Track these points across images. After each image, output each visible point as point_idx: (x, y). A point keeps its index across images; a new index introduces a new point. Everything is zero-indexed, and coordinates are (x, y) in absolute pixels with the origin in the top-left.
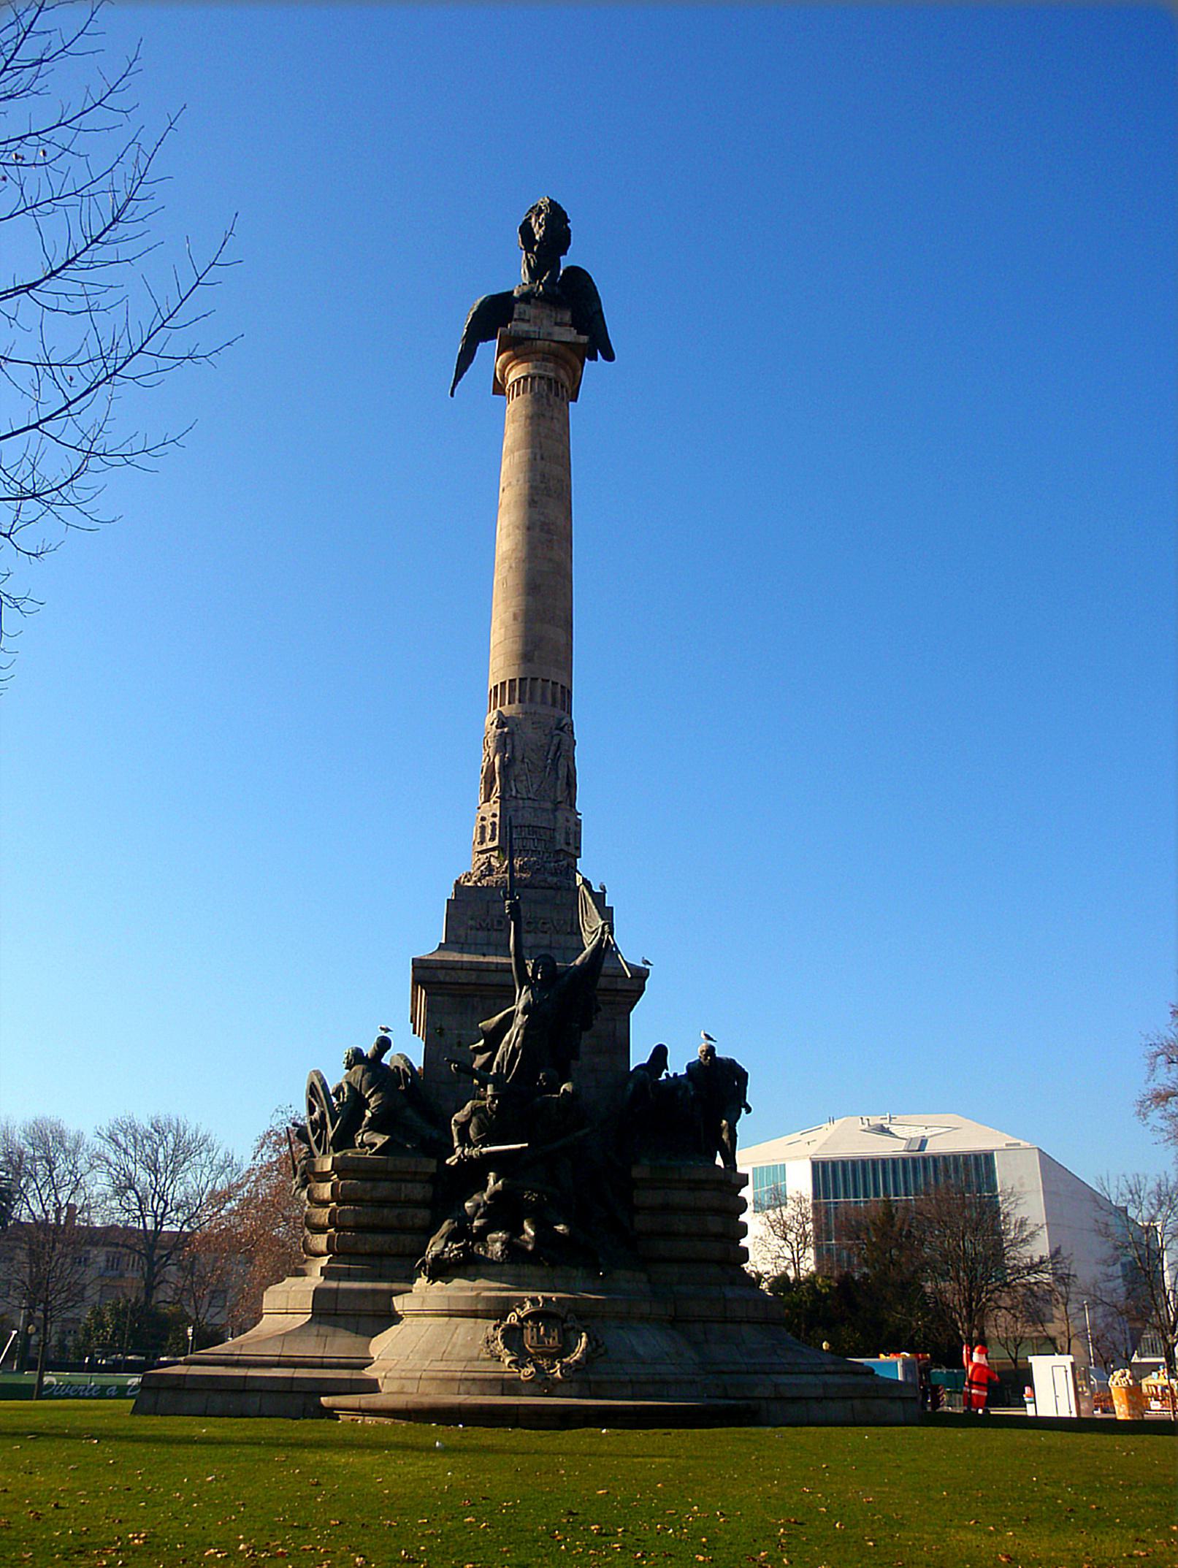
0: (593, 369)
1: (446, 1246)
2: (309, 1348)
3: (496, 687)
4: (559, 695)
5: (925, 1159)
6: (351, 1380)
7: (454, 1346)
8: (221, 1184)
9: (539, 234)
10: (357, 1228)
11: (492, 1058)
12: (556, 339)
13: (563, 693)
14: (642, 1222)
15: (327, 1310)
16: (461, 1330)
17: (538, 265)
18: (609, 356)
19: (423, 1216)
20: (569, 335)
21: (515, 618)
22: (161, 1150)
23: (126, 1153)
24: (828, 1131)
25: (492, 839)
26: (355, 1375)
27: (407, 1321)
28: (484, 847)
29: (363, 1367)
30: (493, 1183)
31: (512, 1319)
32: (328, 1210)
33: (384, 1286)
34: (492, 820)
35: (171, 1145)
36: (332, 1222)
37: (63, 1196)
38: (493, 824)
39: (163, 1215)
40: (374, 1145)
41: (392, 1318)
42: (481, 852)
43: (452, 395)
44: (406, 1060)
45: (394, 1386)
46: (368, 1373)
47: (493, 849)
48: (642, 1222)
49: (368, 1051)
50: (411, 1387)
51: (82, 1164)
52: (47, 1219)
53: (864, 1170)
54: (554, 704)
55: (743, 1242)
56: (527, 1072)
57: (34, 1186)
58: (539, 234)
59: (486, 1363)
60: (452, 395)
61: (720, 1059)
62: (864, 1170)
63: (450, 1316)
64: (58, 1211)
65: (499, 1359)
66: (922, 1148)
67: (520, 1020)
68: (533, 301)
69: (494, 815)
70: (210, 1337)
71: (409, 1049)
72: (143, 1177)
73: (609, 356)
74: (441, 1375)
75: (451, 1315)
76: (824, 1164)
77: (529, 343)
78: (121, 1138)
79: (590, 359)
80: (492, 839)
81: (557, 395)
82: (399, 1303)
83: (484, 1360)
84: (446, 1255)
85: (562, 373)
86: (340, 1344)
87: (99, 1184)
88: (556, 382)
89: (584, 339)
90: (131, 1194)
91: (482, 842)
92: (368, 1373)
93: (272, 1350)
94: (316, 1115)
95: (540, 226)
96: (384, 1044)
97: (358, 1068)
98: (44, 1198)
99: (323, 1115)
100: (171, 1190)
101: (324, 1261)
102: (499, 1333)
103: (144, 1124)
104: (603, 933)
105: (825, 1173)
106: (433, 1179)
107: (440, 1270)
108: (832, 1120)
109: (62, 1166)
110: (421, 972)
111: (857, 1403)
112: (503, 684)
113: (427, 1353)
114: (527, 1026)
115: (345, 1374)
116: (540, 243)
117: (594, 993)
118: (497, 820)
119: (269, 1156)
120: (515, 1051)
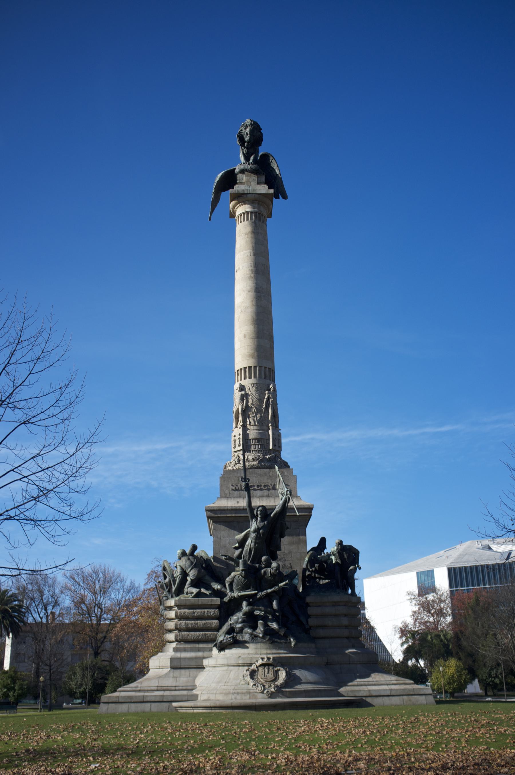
0: (278, 203)
1: (225, 637)
2: (169, 682)
3: (238, 371)
4: (268, 373)
5: (510, 564)
6: (187, 695)
7: (230, 679)
8: (130, 596)
9: (247, 138)
10: (180, 630)
11: (241, 552)
12: (258, 193)
13: (270, 371)
14: (312, 622)
15: (176, 665)
16: (232, 673)
17: (247, 153)
18: (285, 197)
19: (216, 622)
20: (263, 189)
21: (245, 336)
22: (97, 582)
23: (79, 584)
24: (460, 549)
25: (239, 446)
26: (190, 693)
27: (206, 669)
28: (236, 450)
29: (192, 690)
30: (245, 607)
31: (254, 667)
32: (174, 623)
33: (200, 654)
34: (239, 437)
35: (102, 579)
36: (176, 629)
37: (50, 609)
38: (240, 439)
39: (101, 616)
40: (192, 593)
41: (202, 668)
42: (235, 452)
43: (210, 219)
44: (205, 553)
45: (205, 697)
46: (195, 692)
47: (240, 450)
48: (312, 622)
49: (188, 551)
50: (212, 697)
51: (57, 591)
52: (42, 621)
53: (477, 571)
54: (265, 378)
55: (360, 628)
56: (256, 558)
57: (34, 605)
58: (247, 138)
59: (243, 686)
60: (210, 219)
61: (346, 546)
62: (477, 571)
63: (228, 666)
64: (47, 617)
65: (248, 684)
66: (508, 558)
67: (253, 535)
68: (245, 172)
69: (240, 435)
70: (130, 679)
71: (207, 549)
72: (89, 597)
73: (285, 197)
74: (224, 692)
75: (228, 666)
76: (455, 569)
77: (245, 196)
78: (76, 578)
79: (276, 198)
80: (239, 446)
81: (260, 220)
82: (206, 662)
83: (242, 684)
84: (225, 641)
85: (262, 209)
86: (183, 678)
87: (66, 601)
88: (259, 214)
89: (271, 191)
90: (83, 606)
91: (235, 447)
92: (195, 692)
93: (154, 684)
94: (167, 580)
95: (247, 134)
96: (195, 548)
97: (184, 559)
98: (39, 610)
99: (170, 581)
100: (104, 602)
101: (174, 645)
102: (248, 673)
103: (88, 570)
104: (287, 495)
105: (456, 575)
106: (219, 607)
107: (222, 647)
108: (461, 543)
109: (47, 595)
110: (209, 513)
111: (405, 697)
112: (241, 369)
113: (219, 682)
114: (256, 538)
115: (185, 693)
116: (249, 142)
117: (282, 524)
118: (241, 437)
119: (152, 584)
120: (250, 550)
